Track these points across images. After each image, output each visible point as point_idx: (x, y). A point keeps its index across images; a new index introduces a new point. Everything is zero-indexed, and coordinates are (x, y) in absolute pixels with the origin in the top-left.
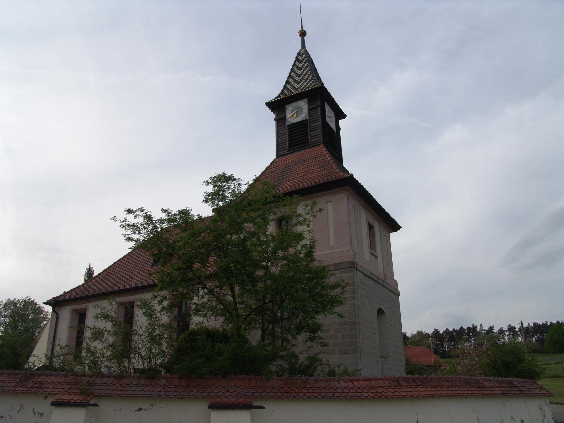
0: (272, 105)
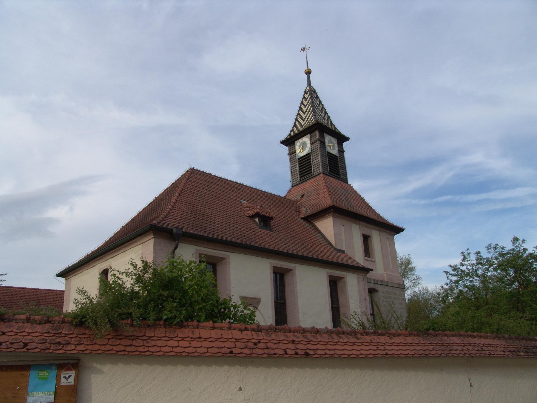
0: (284, 142)
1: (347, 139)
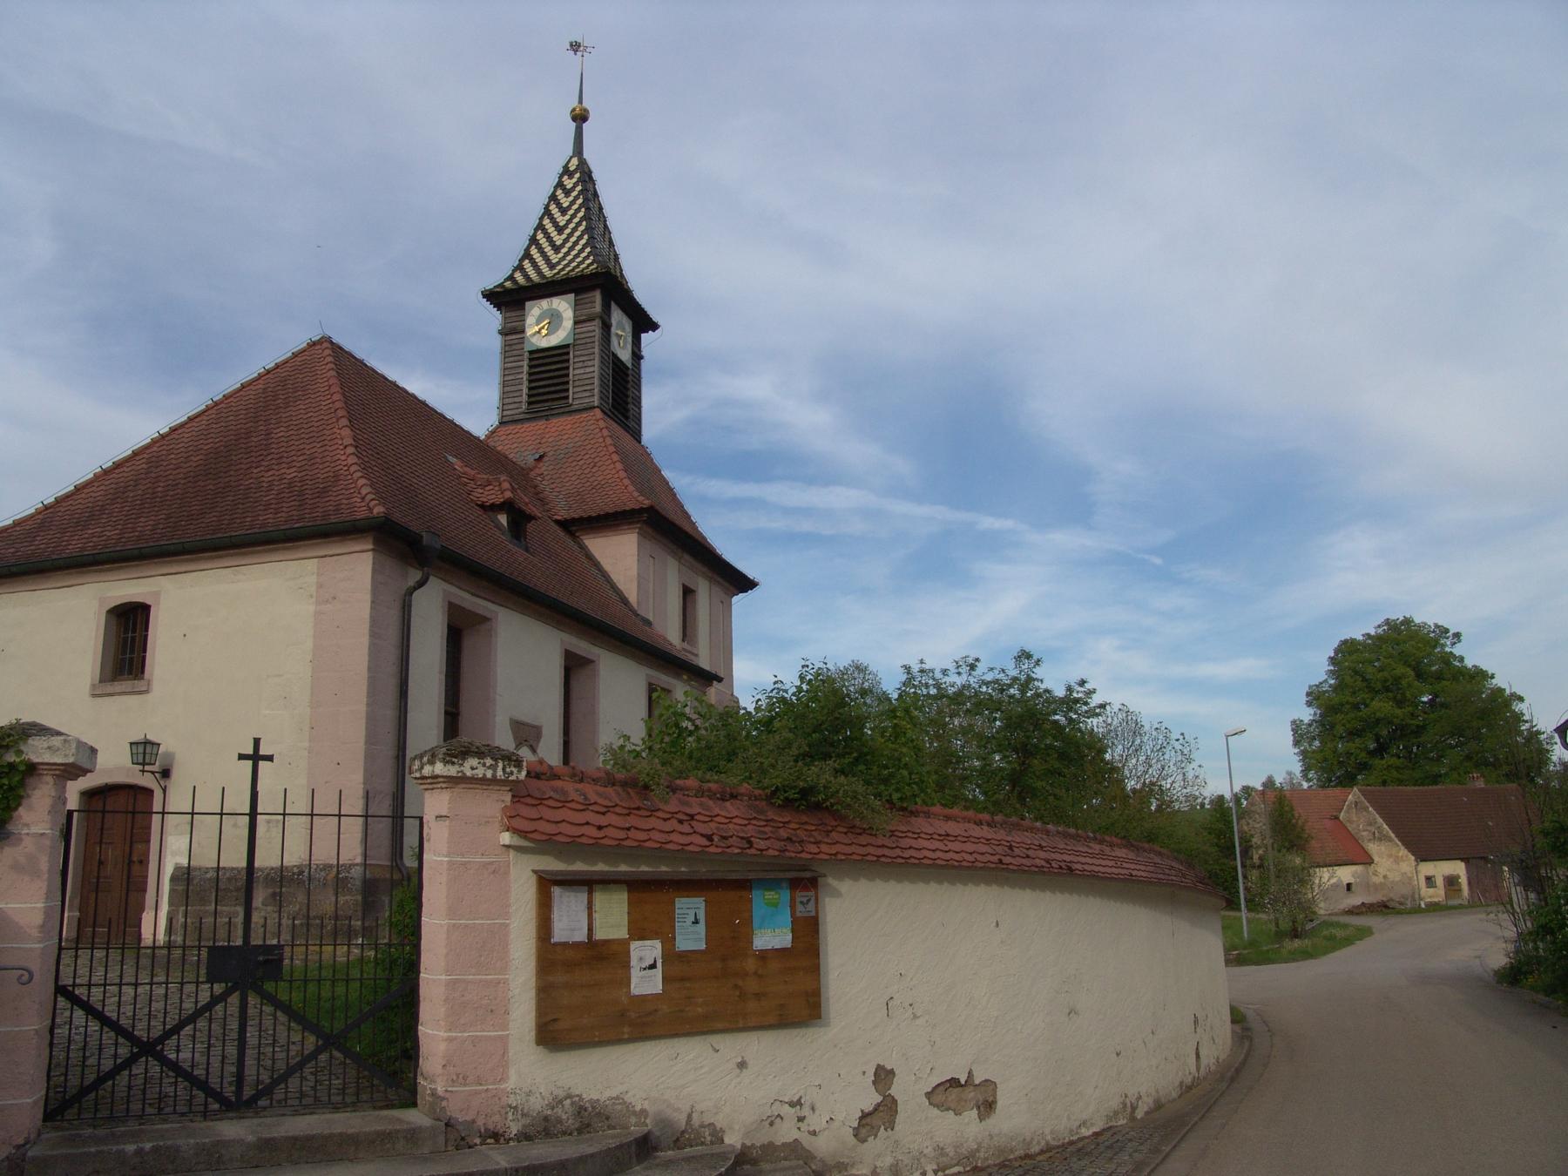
1: (654, 326)
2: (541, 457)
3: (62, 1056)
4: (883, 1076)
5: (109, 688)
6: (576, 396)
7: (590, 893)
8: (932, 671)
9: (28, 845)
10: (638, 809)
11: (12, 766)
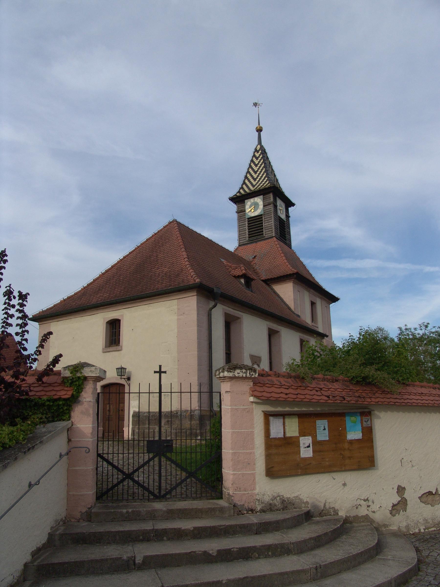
1: (293, 205)
2: (255, 257)
3: (101, 477)
4: (401, 490)
5: (109, 349)
6: (266, 233)
7: (284, 419)
8: (410, 329)
9: (86, 405)
10: (301, 386)
11: (79, 378)
